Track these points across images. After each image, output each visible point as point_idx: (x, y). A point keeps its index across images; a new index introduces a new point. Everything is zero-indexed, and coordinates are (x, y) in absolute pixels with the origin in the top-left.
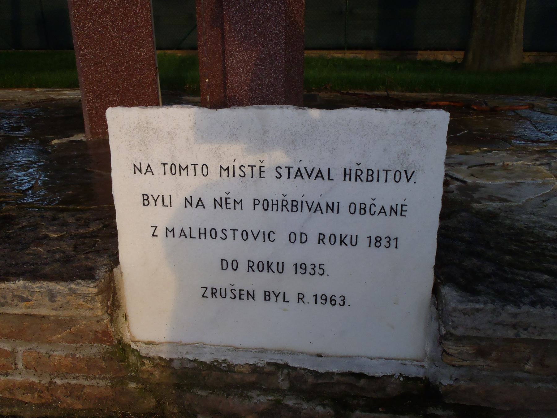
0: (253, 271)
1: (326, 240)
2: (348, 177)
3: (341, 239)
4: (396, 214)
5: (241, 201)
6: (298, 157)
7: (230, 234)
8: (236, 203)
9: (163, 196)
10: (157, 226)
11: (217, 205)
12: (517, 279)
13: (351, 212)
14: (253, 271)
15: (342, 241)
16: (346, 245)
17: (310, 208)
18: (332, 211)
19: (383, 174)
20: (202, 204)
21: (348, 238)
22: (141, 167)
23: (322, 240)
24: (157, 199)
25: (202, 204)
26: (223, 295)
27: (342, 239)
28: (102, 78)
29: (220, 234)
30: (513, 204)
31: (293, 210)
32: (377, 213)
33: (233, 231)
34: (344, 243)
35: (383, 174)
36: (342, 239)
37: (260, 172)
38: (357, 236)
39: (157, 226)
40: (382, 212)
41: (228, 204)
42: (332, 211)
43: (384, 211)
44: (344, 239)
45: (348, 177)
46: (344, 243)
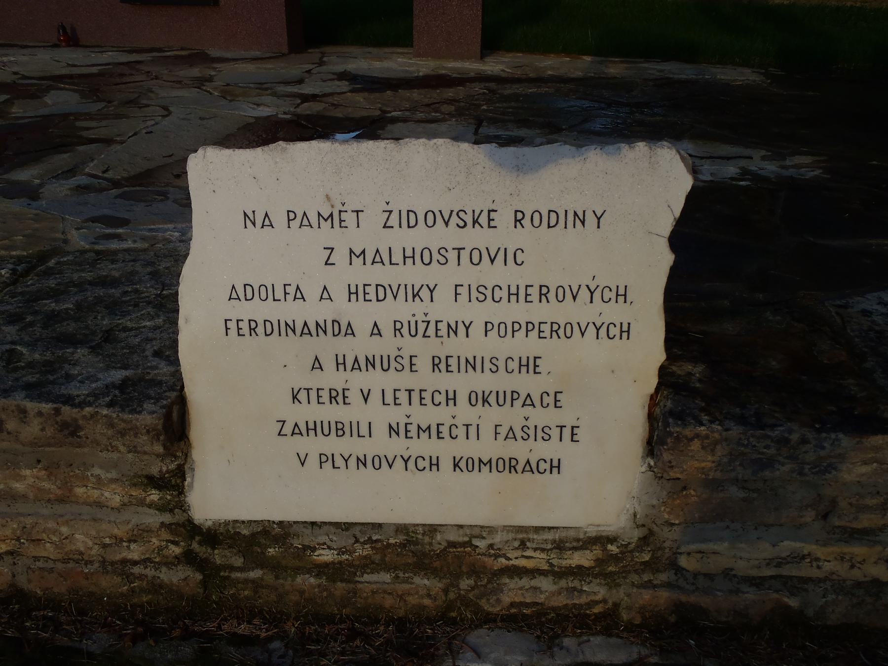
0: (338, 403)
1: (526, 222)
2: (353, 297)
3: (474, 219)
7: (452, 256)
10: (384, 227)
12: (680, 381)
14: (338, 403)
15: (252, 330)
16: (463, 322)
21: (493, 396)
22: (351, 256)
23: (520, 221)
26: (385, 366)
27: (295, 394)
30: (732, 411)
33: (356, 213)
36: (485, 397)
38: (438, 457)
39: (384, 227)
41: (458, 294)
43: (351, 333)
44: (487, 398)
45: (353, 297)
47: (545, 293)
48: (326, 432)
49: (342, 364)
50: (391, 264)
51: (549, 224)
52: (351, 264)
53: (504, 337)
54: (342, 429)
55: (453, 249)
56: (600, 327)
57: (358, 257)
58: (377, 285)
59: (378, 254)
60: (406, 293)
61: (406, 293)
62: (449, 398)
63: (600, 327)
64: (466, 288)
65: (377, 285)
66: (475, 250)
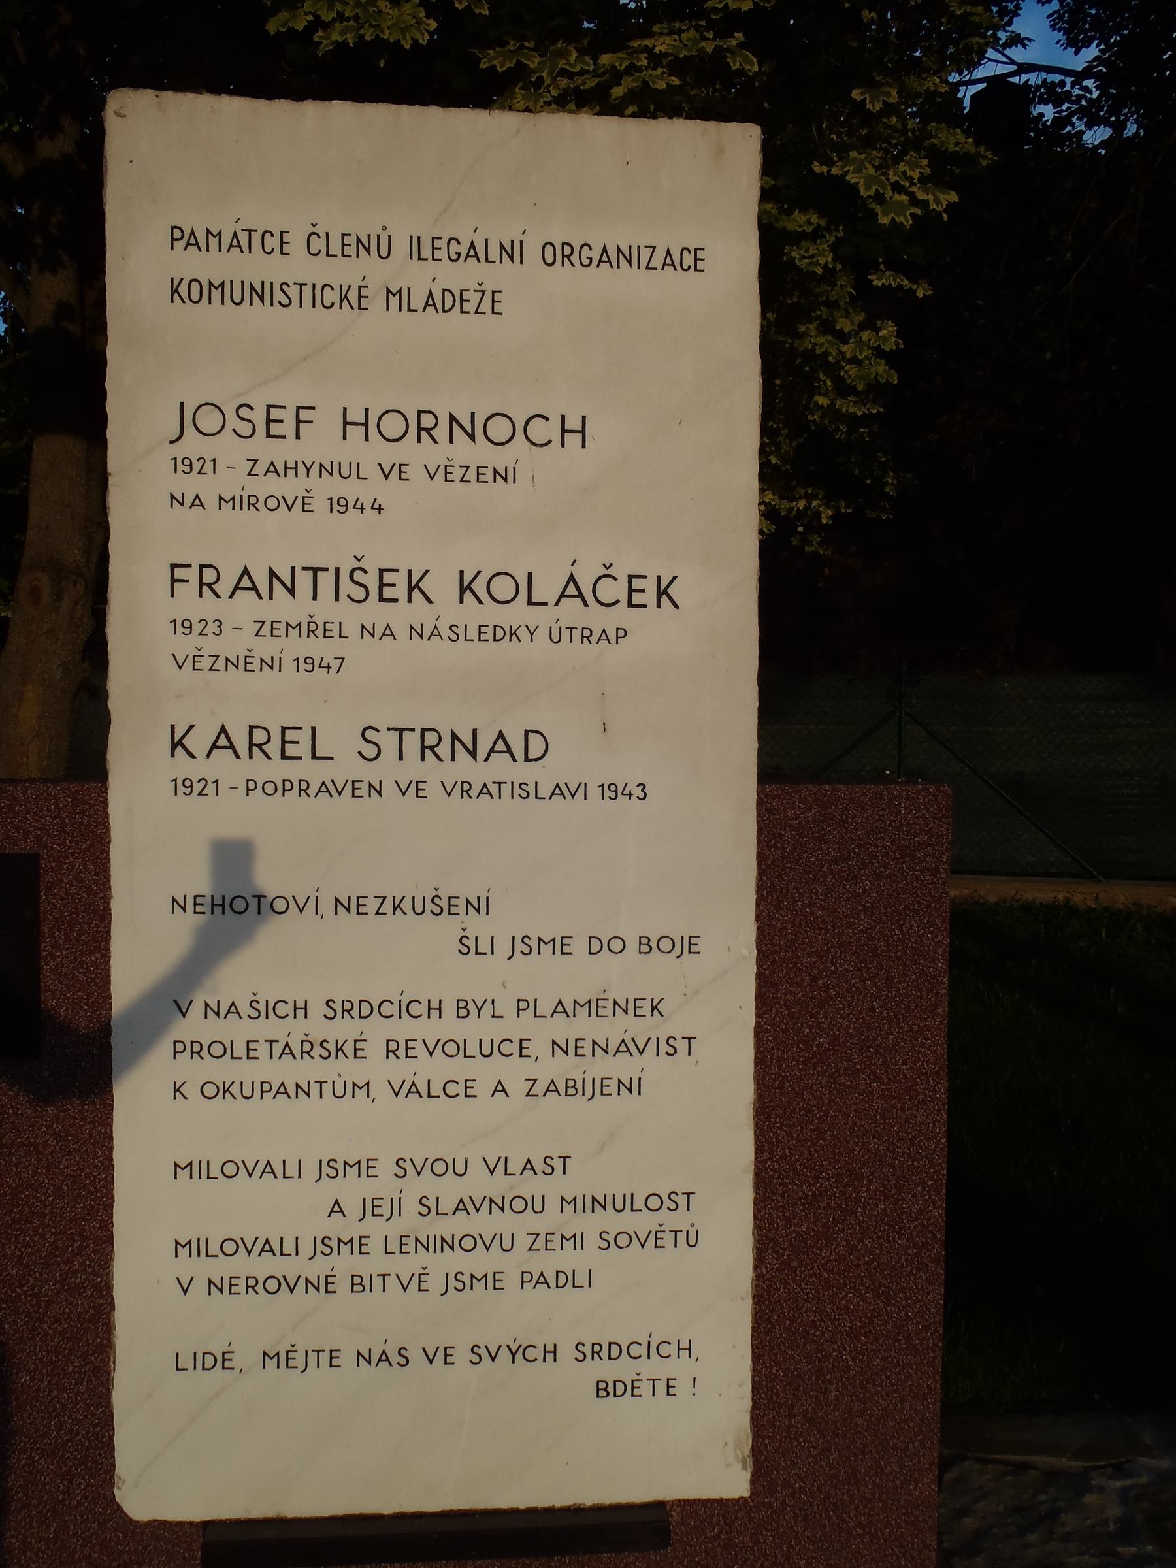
4: (512, 261)
5: (220, 233)
6: (337, 1207)
8: (454, 423)
9: (220, 250)
11: (468, 740)
13: (552, 248)
17: (470, 431)
18: (511, 258)
19: (377, 1281)
20: (577, 594)
24: (343, 789)
25: (577, 594)
28: (767, 1215)
29: (664, 1047)
31: (533, 600)
32: (595, 262)
34: (180, 1092)
35: (377, 1281)
37: (668, 1387)
40: (472, 257)
42: (511, 258)
46: (180, 1092)
47: (308, 1050)
48: (619, 1206)
49: (361, 424)
50: (314, 757)
51: (463, 477)
52: (173, 913)
53: (451, 1041)
54: (574, 1087)
55: (683, 1038)
56: (311, 467)
57: (294, 628)
58: (495, 627)
59: (418, 1243)
60: (314, 294)
61: (314, 294)
62: (384, 582)
63: (311, 467)
64: (332, 571)
65: (495, 627)
66: (434, 421)
